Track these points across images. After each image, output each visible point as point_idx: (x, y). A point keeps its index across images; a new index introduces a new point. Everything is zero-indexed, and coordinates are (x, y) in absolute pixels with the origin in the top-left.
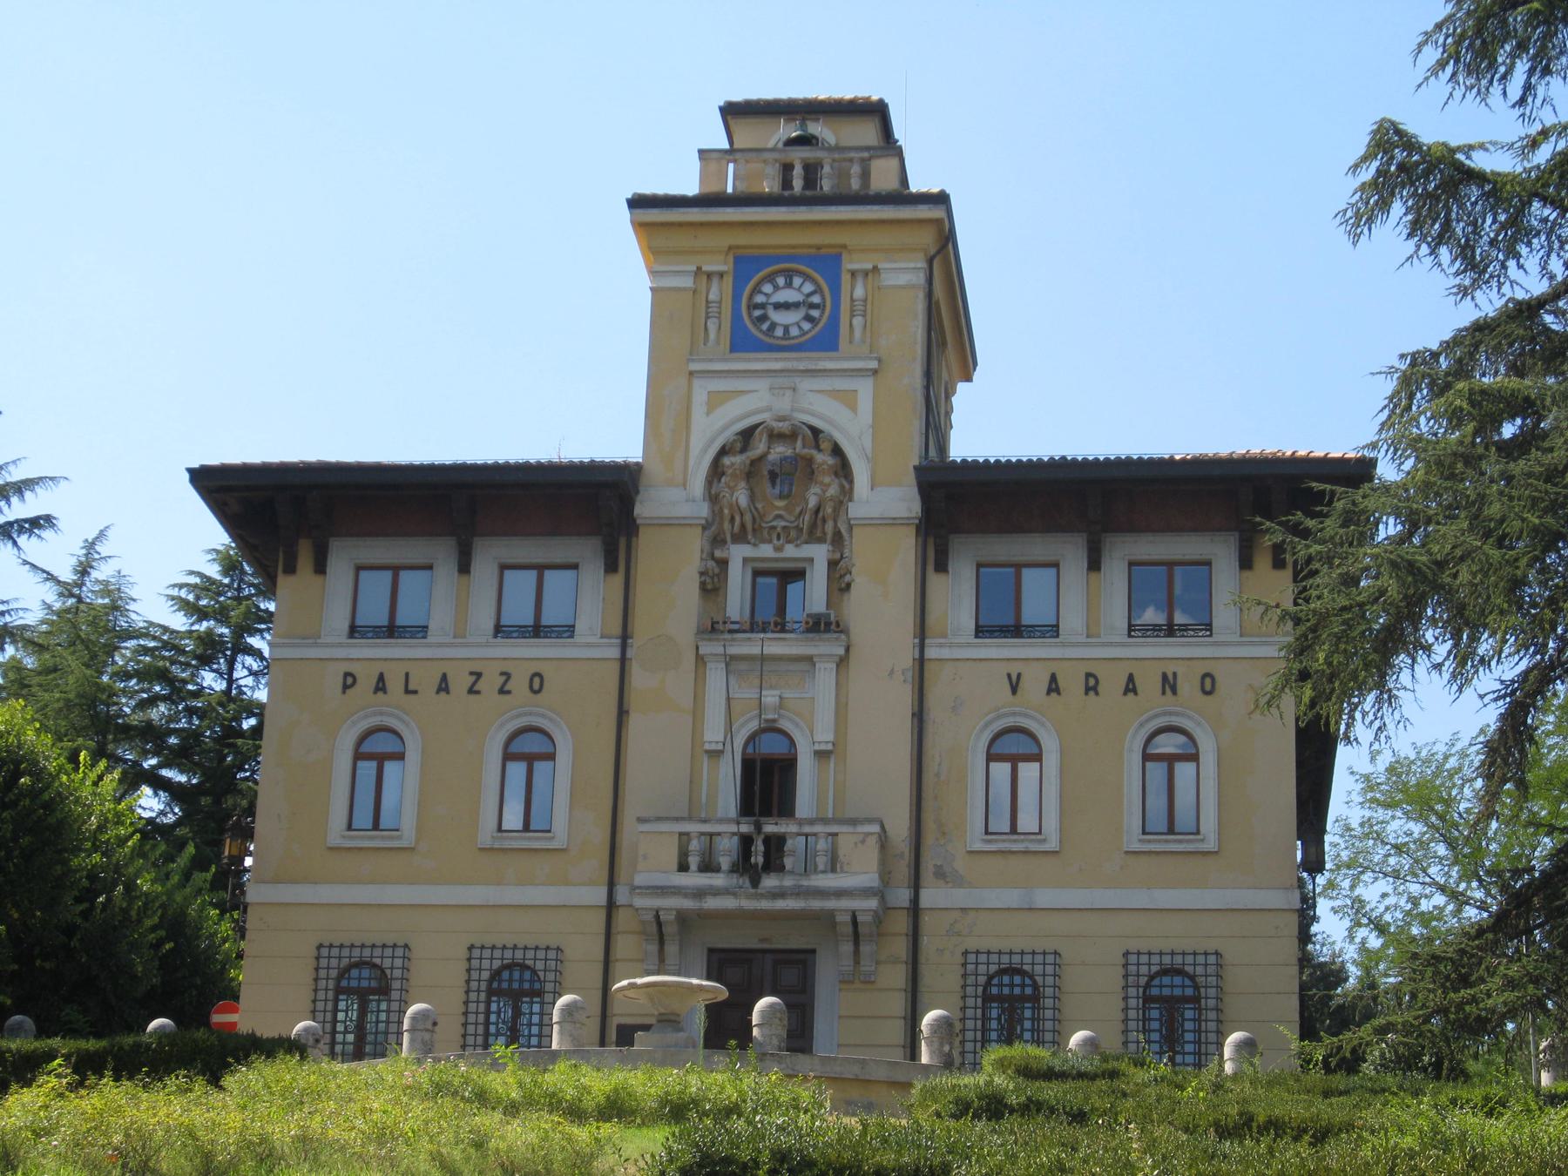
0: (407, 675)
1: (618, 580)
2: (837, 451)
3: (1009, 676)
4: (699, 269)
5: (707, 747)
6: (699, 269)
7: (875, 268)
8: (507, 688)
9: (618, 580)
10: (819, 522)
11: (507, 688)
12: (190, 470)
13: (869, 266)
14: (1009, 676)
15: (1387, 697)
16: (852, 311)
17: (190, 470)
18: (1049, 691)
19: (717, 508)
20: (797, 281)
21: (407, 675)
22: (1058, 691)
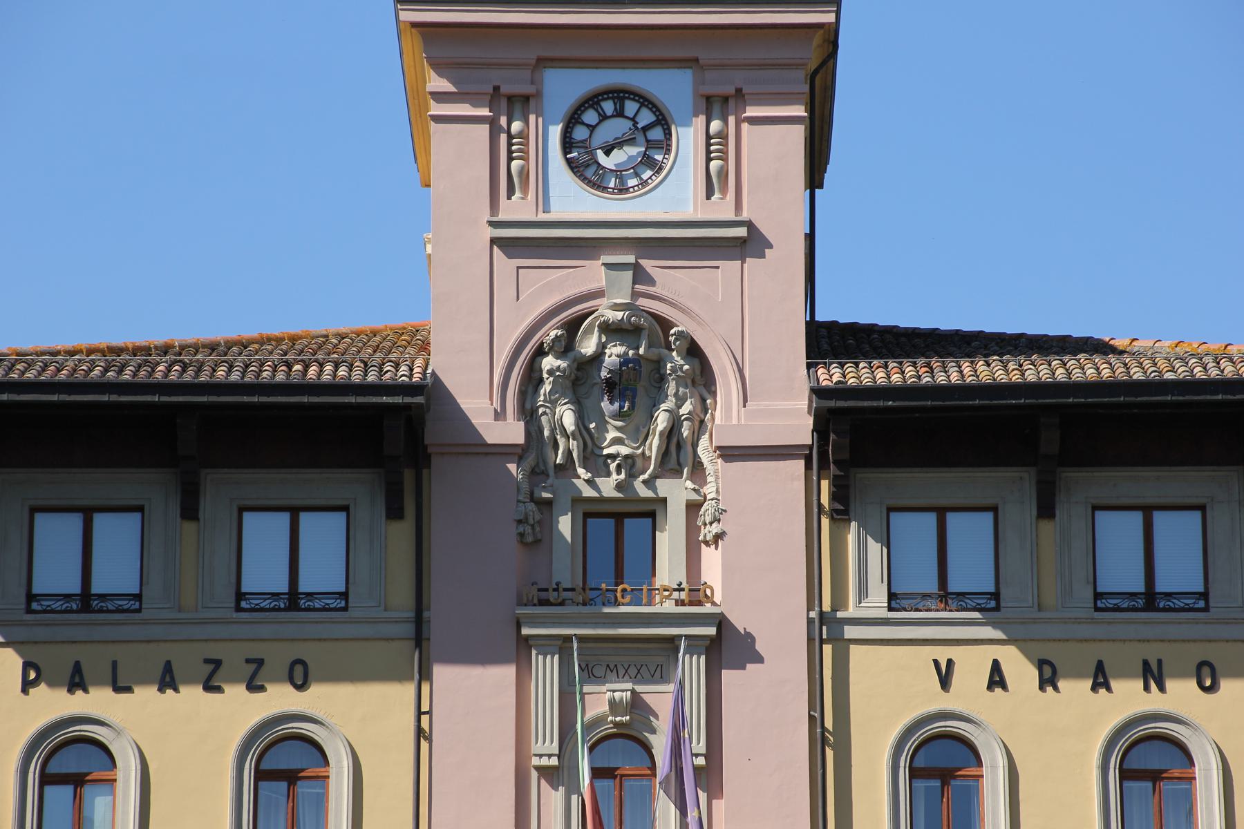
0: (114, 664)
1: (402, 532)
2: (693, 351)
3: (936, 662)
4: (496, 89)
5: (536, 761)
6: (496, 89)
7: (739, 91)
8: (211, 667)
9: (402, 532)
10: (673, 448)
11: (211, 667)
12: (759, 659)
13: (730, 90)
14: (936, 662)
15: (429, 467)
16: (510, 152)
17: (759, 659)
18: (990, 687)
19: (533, 429)
20: (631, 107)
21: (114, 664)
22: (1004, 687)
